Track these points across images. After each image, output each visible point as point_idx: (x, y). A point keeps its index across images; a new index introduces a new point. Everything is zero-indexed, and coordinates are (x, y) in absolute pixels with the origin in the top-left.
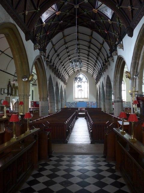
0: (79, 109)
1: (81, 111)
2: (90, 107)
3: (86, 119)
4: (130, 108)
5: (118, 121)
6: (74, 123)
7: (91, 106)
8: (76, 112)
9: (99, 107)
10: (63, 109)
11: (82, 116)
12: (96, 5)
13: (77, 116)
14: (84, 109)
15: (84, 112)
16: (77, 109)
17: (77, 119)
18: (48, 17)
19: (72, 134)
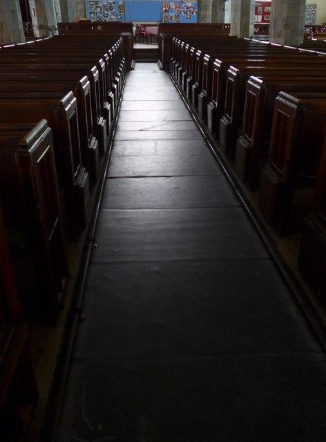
0: (134, 29)
1: (143, 37)
2: (174, 21)
3: (166, 68)
4: (274, 37)
5: (96, 80)
6: (122, 85)
7: (177, 17)
8: (125, 38)
9: (209, 20)
10: (72, 26)
11: (146, 57)
12: (95, 225)
13: (127, 59)
14: (154, 30)
15: (151, 42)
16: (128, 27)
17: (128, 69)
18: (151, 203)
19: (118, 148)
